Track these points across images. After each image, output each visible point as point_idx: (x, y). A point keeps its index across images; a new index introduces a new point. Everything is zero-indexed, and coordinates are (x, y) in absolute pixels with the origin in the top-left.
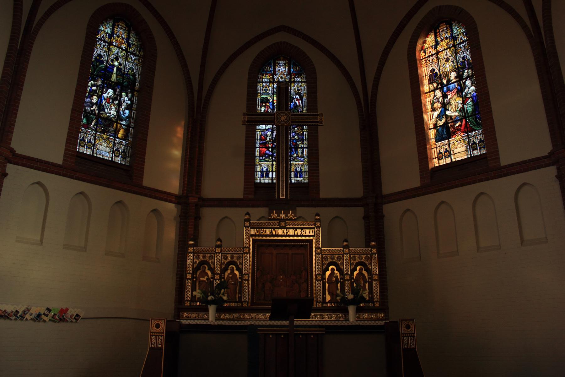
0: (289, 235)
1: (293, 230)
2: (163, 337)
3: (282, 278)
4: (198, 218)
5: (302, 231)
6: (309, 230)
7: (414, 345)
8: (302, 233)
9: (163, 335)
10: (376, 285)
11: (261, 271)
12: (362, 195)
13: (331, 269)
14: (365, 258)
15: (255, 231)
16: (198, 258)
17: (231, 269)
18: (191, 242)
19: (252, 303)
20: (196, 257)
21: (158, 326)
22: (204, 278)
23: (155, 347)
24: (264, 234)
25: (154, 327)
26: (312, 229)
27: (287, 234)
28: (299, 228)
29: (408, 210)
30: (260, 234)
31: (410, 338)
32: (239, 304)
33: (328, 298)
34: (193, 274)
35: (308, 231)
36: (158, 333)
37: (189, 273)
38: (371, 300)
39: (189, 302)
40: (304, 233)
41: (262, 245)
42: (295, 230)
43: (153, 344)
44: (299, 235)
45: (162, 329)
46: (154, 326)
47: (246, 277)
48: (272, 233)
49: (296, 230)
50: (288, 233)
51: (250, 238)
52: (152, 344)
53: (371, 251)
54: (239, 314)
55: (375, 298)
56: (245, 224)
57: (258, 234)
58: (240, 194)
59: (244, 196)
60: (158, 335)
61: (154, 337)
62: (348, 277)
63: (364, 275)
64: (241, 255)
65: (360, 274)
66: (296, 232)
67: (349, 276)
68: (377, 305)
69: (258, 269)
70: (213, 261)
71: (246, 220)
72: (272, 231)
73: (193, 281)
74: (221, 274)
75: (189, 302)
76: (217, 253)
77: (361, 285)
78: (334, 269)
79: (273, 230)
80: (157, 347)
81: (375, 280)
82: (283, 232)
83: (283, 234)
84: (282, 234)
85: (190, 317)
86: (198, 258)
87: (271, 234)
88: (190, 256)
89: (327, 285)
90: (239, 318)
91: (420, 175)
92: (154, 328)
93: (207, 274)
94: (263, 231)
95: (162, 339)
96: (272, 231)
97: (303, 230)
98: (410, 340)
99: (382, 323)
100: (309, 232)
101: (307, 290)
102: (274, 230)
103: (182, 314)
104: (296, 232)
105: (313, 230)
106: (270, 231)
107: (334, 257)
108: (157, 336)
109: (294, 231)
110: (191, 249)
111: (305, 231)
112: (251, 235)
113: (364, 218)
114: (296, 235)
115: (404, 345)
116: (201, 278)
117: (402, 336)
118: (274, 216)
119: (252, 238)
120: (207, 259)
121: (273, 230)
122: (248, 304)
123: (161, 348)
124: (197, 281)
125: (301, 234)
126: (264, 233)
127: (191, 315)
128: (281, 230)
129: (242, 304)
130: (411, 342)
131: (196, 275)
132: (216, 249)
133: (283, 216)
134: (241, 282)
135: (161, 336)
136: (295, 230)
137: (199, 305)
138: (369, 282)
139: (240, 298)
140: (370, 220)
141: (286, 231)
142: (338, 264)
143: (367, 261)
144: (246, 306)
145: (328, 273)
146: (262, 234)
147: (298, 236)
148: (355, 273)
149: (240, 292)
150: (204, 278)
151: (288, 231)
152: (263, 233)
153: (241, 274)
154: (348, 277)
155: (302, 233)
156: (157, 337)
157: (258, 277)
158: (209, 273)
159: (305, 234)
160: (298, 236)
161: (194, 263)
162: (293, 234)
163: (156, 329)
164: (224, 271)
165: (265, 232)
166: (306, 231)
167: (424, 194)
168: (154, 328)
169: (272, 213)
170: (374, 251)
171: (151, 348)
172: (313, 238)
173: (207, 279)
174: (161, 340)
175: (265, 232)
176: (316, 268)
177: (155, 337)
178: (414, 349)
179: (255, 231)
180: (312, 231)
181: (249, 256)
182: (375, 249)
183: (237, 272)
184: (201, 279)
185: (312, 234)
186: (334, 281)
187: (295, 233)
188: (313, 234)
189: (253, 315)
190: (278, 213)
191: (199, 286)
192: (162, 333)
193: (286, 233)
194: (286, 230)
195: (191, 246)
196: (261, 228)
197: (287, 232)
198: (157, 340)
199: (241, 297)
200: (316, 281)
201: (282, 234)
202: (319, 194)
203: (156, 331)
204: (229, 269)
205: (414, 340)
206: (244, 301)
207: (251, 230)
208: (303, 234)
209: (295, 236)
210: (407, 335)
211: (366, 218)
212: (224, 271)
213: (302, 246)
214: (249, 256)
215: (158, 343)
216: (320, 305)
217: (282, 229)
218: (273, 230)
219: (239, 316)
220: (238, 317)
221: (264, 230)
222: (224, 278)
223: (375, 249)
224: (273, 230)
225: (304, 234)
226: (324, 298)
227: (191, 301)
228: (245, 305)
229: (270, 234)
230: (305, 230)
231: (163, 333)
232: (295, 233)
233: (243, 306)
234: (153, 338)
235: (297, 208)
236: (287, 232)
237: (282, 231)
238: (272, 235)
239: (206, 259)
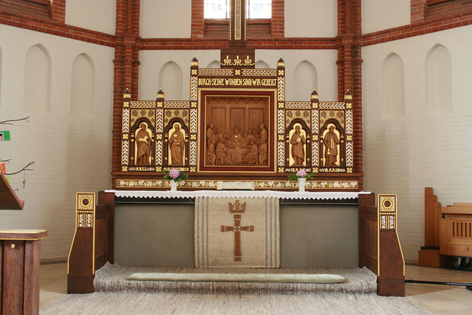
0: (245, 86)
1: (250, 79)
2: (92, 215)
3: (237, 138)
4: (136, 63)
5: (261, 81)
6: (270, 80)
7: (393, 225)
8: (261, 83)
9: (93, 213)
10: (349, 147)
11: (212, 129)
12: (337, 35)
13: (296, 127)
14: (338, 114)
15: (204, 81)
16: (135, 114)
17: (175, 128)
18: (128, 96)
19: (202, 168)
20: (133, 113)
21: (86, 202)
22: (143, 138)
23: (84, 227)
24: (215, 85)
25: (81, 203)
26: (274, 79)
27: (243, 85)
28: (258, 77)
29: (393, 54)
30: (210, 85)
31: (389, 217)
32: (186, 169)
33: (292, 161)
34: (130, 134)
35: (268, 81)
36: (86, 210)
37: (125, 133)
38: (343, 165)
39: (127, 167)
40: (264, 83)
41: (214, 98)
42: (253, 79)
43: (81, 223)
44: (258, 86)
45: (92, 205)
46: (82, 202)
47: (193, 137)
48: (225, 84)
49: (254, 80)
50: (244, 84)
51: (198, 89)
52: (79, 224)
53: (345, 106)
54: (185, 181)
55: (347, 163)
56: (191, 72)
57: (207, 84)
58: (186, 33)
59: (191, 36)
60: (86, 212)
61: (82, 215)
62: (315, 138)
63: (335, 135)
64: (188, 110)
65: (331, 133)
66: (254, 83)
67: (317, 136)
68: (350, 171)
69: (208, 127)
70: (154, 118)
71: (193, 68)
72: (224, 81)
73: (130, 143)
74: (163, 134)
75: (127, 167)
76: (158, 108)
77: (332, 147)
78: (300, 128)
79: (225, 79)
80: (86, 227)
81: (348, 141)
82: (238, 83)
83: (238, 85)
84: (237, 85)
85: (128, 186)
86: (135, 114)
87: (224, 85)
88: (126, 113)
89: (291, 146)
90: (186, 186)
91: (411, 10)
92: (81, 206)
93: (148, 135)
94: (214, 81)
95: (91, 218)
96: (224, 81)
97: (263, 80)
98: (390, 219)
99: (354, 195)
100: (271, 83)
101: (267, 152)
102: (227, 80)
103: (118, 182)
104: (254, 83)
105: (275, 80)
106: (223, 81)
107: (299, 113)
108: (85, 214)
109: (252, 81)
110: (126, 104)
111: (265, 81)
112: (199, 86)
113: (338, 63)
114: (254, 86)
115: (382, 226)
116: (140, 138)
117: (380, 215)
118: (227, 61)
119: (200, 89)
120: (146, 116)
121: (226, 80)
122: (196, 169)
123: (91, 229)
124: (135, 141)
125: (260, 85)
126: (215, 84)
127: (129, 183)
128: (236, 79)
129: (190, 169)
130: (390, 221)
131: (134, 135)
132: (156, 103)
133: (238, 62)
134: (188, 143)
135: (91, 214)
136: (253, 79)
137: (138, 170)
138: (340, 143)
139: (187, 162)
140: (345, 66)
141: (242, 81)
142: (304, 122)
143: (340, 117)
144: (195, 171)
145: (292, 132)
146: (213, 84)
147: (256, 87)
148: (325, 132)
149: (187, 155)
150: (143, 138)
151: (245, 81)
152: (213, 83)
153: (188, 133)
154: (315, 138)
155: (261, 83)
156: (85, 215)
157: (208, 136)
158: (149, 131)
159: (265, 85)
160: (256, 87)
161: (131, 121)
162: (251, 85)
163: (84, 206)
164: (166, 130)
165: (216, 83)
166: (266, 81)
167: (415, 34)
168: (81, 205)
169: (224, 59)
170: (349, 106)
171: (79, 228)
172: (275, 89)
173: (148, 140)
174: (90, 219)
175: (216, 83)
176: (280, 128)
177: (83, 215)
178: (394, 230)
179: (204, 81)
180: (274, 81)
181: (198, 112)
182: (351, 104)
183: (183, 131)
184: (141, 139)
185: (273, 85)
186: (299, 142)
187: (252, 83)
188: (275, 85)
189: (203, 183)
190: (233, 59)
191: (138, 148)
192: (91, 210)
193: (242, 83)
194: (241, 79)
195: (127, 100)
196: (212, 77)
197: (243, 83)
198: (85, 219)
199: (188, 161)
200: (277, 142)
201: (237, 84)
202: (283, 32)
203: (86, 209)
204: (174, 127)
205: (393, 219)
206: (192, 166)
207: (199, 79)
208: (263, 85)
209: (252, 86)
210: (385, 214)
211: (340, 62)
212: (166, 130)
213: (261, 99)
214: (198, 112)
215: (87, 222)
216: (281, 170)
217: (236, 78)
218: (226, 80)
219: (186, 184)
220: (184, 185)
221: (215, 79)
222: (167, 138)
223: (351, 104)
224: (225, 79)
225: (264, 84)
226: (287, 163)
227: (129, 166)
228: (193, 170)
229: (222, 85)
230: (265, 80)
231: (93, 210)
232: (252, 83)
233: (191, 171)
234: (80, 217)
235: (257, 51)
236: (243, 83)
237: (237, 80)
238: (225, 86)
239: (145, 116)
